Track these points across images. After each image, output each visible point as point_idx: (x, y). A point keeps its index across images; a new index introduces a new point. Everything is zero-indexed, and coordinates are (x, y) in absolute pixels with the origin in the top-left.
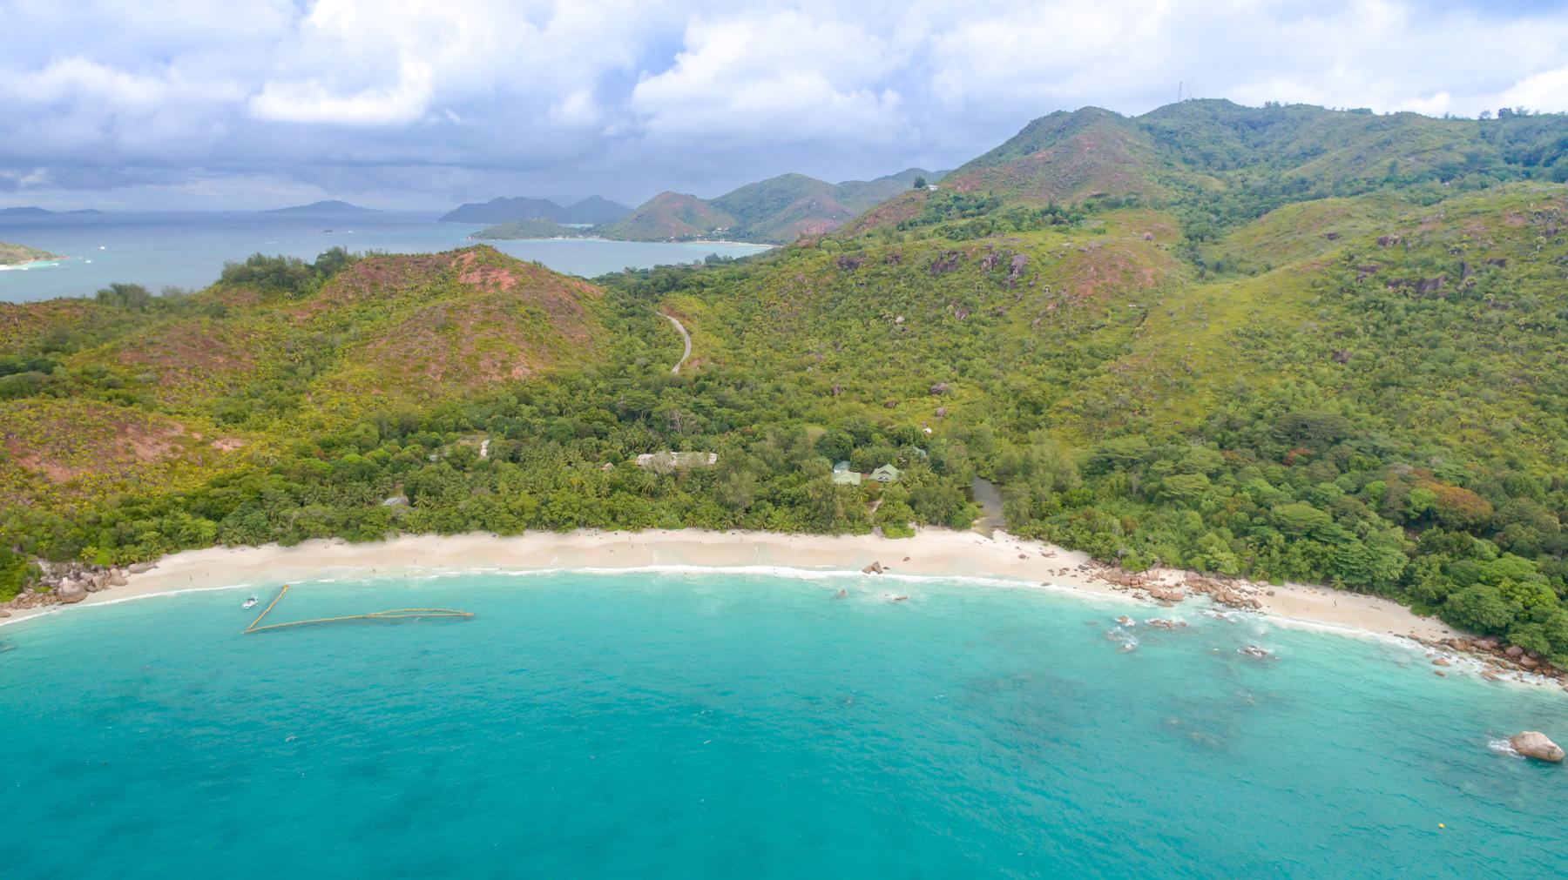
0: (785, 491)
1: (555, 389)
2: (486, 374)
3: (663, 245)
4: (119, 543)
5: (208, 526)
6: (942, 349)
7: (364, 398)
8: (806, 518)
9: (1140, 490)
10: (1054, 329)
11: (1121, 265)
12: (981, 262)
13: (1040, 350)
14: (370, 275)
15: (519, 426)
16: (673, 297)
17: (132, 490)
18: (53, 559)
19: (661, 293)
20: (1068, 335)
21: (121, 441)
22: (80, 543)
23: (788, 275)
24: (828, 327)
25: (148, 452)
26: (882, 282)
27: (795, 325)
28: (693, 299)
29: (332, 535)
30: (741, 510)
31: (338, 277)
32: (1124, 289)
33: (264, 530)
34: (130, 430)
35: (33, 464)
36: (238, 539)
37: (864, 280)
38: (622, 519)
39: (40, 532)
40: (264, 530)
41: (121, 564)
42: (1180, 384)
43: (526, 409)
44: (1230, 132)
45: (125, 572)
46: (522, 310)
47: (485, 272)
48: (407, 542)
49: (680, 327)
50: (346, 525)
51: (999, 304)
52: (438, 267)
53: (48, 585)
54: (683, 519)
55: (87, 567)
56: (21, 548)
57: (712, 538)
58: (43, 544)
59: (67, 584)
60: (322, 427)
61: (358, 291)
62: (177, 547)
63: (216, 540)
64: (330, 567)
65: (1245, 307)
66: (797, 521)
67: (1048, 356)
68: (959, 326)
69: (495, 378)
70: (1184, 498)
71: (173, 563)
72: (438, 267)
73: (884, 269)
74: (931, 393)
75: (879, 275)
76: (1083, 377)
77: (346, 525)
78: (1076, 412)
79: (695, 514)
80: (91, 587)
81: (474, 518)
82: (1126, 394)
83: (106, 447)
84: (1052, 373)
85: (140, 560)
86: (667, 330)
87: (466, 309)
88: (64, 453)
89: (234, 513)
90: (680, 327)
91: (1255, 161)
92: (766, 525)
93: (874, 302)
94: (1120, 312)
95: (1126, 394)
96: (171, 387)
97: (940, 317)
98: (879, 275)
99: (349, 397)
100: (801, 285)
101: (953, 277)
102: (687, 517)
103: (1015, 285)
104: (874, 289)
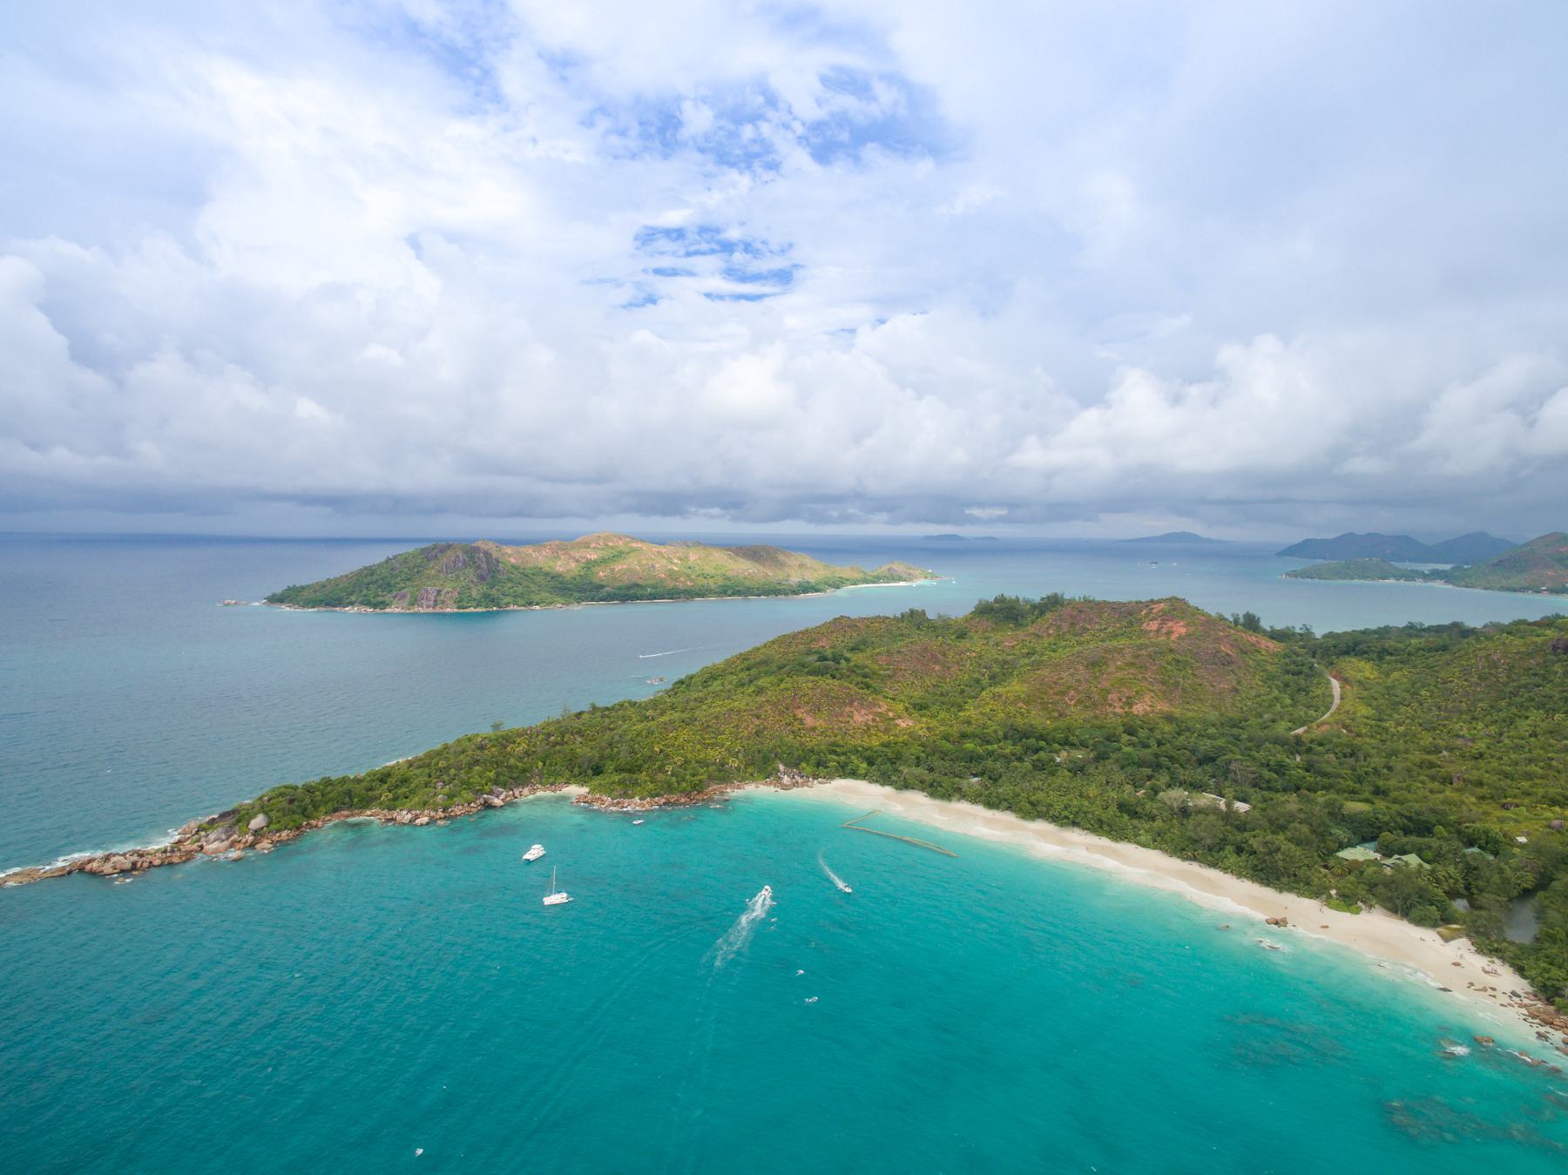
1: (1167, 728)
3: (1530, 596)
4: (818, 765)
8: (1255, 868)
9: (1510, 900)
18: (786, 765)
19: (1338, 655)
22: (800, 759)
23: (1481, 653)
25: (860, 718)
29: (923, 790)
35: (800, 714)
38: (1106, 828)
41: (815, 777)
43: (1125, 737)
47: (1164, 622)
48: (964, 806)
50: (931, 785)
57: (1176, 863)
59: (786, 780)
60: (969, 723)
61: (1059, 627)
62: (844, 776)
63: (864, 777)
64: (913, 810)
69: (1118, 710)
71: (839, 783)
77: (931, 785)
80: (796, 784)
87: (1120, 651)
88: (816, 710)
89: (885, 765)
102: (1158, 841)
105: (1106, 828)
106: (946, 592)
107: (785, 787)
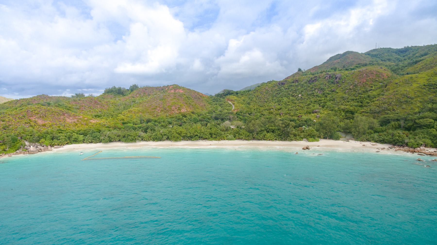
0: (271, 128)
2: (173, 111)
5: (81, 137)
6: (315, 101)
7: (137, 115)
8: (279, 135)
10: (354, 93)
11: (375, 73)
12: (325, 77)
13: (350, 98)
14: (143, 91)
15: (181, 120)
16: (228, 97)
17: (61, 128)
18: (30, 142)
20: (359, 94)
21: (62, 117)
24: (276, 100)
26: (293, 88)
27: (266, 100)
28: (234, 96)
30: (255, 133)
31: (135, 91)
32: (377, 79)
33: (98, 138)
34: (66, 115)
36: (90, 140)
37: (287, 87)
38: (214, 136)
39: (27, 133)
40: (98, 138)
41: (52, 146)
42: (407, 101)
44: (395, 54)
45: (53, 148)
46: (185, 96)
47: (175, 90)
49: (231, 103)
50: (124, 137)
51: (333, 88)
52: (162, 89)
53: (27, 149)
54: (235, 137)
55: (41, 145)
56: (21, 138)
58: (28, 137)
59: (32, 148)
63: (83, 142)
65: (425, 78)
66: (275, 136)
67: (353, 100)
68: (320, 95)
69: (176, 112)
70: (424, 126)
72: (162, 89)
73: (293, 84)
74: (313, 113)
75: (292, 86)
76: (368, 103)
78: (367, 113)
79: (239, 134)
80: (40, 151)
81: (165, 135)
82: (386, 105)
83: (57, 117)
84: (356, 104)
85: (58, 145)
86: (227, 104)
88: (43, 117)
90: (231, 103)
91: (405, 60)
92: (264, 138)
93: (291, 93)
94: (376, 86)
95: (386, 105)
96: (83, 110)
97: (313, 93)
98: (292, 86)
99: (134, 114)
100: (267, 90)
101: (316, 83)
103: (337, 83)
104: (290, 89)
105: (214, 136)
106: (68, 94)
107: (30, 152)
